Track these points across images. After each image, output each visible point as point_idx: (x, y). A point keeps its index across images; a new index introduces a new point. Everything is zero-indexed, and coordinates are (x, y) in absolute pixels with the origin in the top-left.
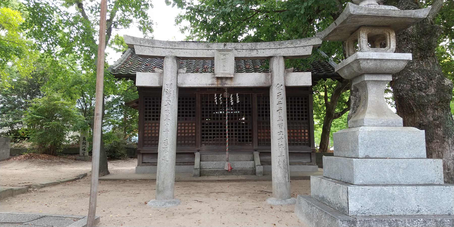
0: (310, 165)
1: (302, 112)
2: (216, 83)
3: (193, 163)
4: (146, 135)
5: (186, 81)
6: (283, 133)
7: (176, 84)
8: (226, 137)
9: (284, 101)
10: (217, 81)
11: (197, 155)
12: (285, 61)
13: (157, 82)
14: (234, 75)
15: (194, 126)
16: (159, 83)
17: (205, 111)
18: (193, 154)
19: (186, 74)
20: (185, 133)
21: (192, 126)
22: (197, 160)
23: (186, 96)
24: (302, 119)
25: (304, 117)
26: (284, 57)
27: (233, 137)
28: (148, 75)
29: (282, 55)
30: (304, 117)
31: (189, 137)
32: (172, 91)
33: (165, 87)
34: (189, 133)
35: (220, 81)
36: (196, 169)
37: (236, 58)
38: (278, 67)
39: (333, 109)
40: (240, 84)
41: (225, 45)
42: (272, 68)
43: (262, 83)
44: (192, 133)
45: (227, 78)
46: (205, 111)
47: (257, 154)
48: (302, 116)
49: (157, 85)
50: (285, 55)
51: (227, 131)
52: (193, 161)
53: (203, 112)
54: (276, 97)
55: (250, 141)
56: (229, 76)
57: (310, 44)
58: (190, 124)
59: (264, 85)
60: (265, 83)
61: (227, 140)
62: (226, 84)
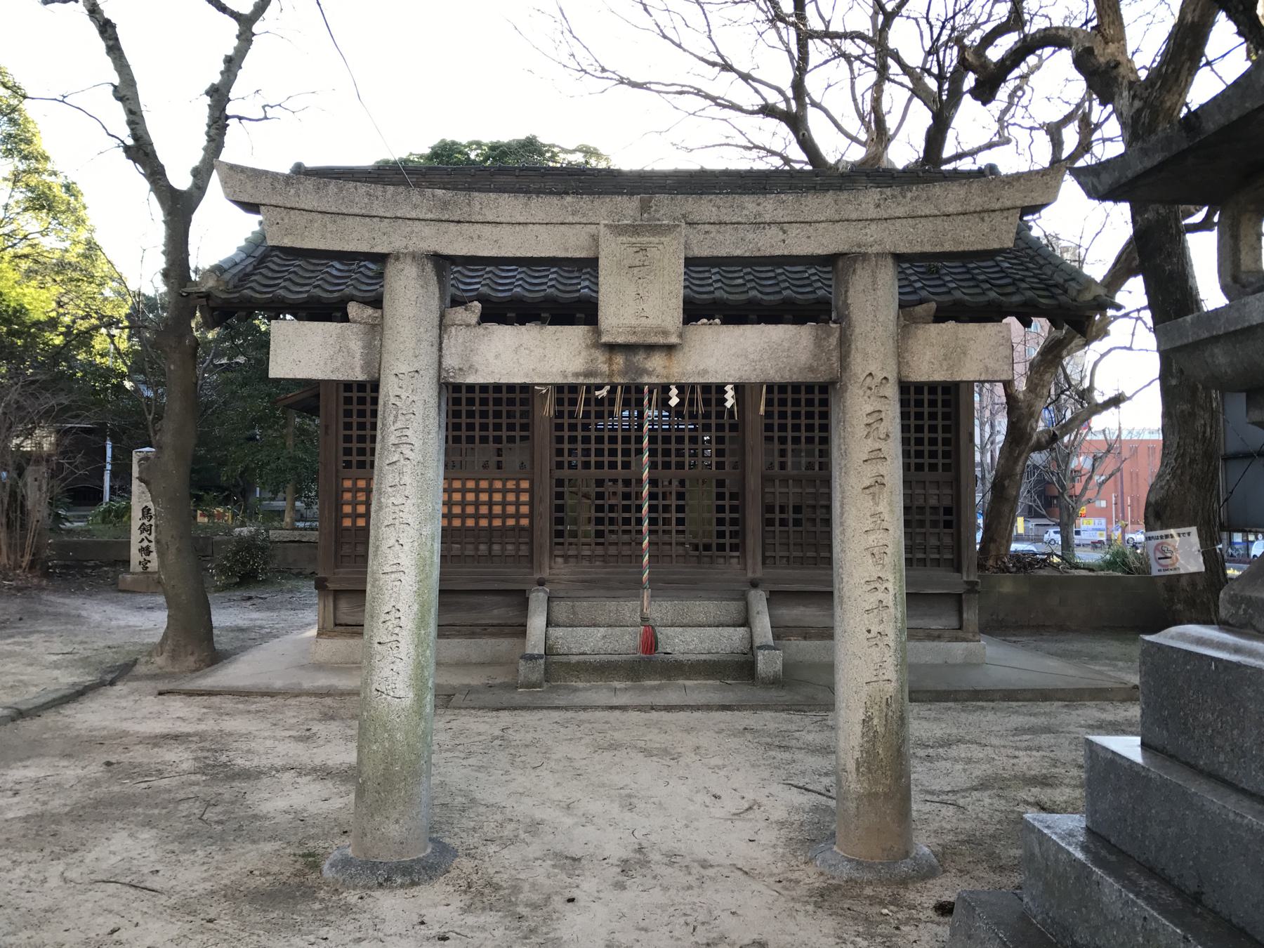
0: (957, 639)
1: (933, 442)
2: (604, 368)
3: (520, 630)
4: (347, 523)
5: (477, 360)
6: (890, 586)
7: (432, 372)
8: (640, 532)
9: (894, 449)
10: (610, 361)
11: (538, 600)
12: (902, 277)
13: (358, 362)
14: (681, 336)
15: (524, 491)
16: (367, 365)
17: (566, 434)
18: (521, 600)
19: (480, 330)
20: (490, 516)
21: (518, 491)
22: (537, 622)
23: (479, 418)
24: (933, 467)
25: (940, 461)
26: (898, 258)
27: (669, 532)
28: (321, 332)
29: (889, 247)
30: (940, 461)
31: (504, 530)
32: (419, 404)
33: (390, 389)
34: (504, 516)
35: (620, 360)
36: (532, 658)
37: (690, 262)
38: (873, 301)
39: (1032, 415)
40: (705, 372)
41: (645, 208)
42: (847, 306)
43: (801, 370)
44: (517, 516)
45: (651, 348)
46: (566, 434)
47: (758, 600)
48: (933, 455)
49: (358, 374)
50: (903, 249)
51: (646, 508)
52: (521, 621)
53: (560, 440)
54: (861, 431)
55: (734, 548)
56: (661, 340)
57: (1008, 204)
58: (510, 485)
59: (810, 378)
60: (811, 369)
61: (646, 441)
62: (645, 372)
